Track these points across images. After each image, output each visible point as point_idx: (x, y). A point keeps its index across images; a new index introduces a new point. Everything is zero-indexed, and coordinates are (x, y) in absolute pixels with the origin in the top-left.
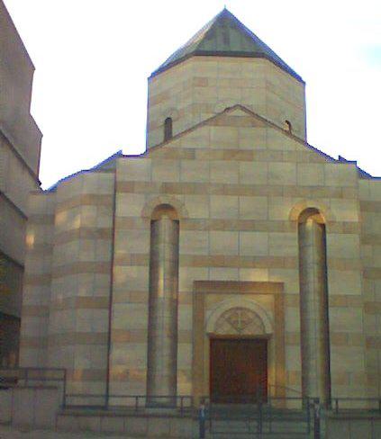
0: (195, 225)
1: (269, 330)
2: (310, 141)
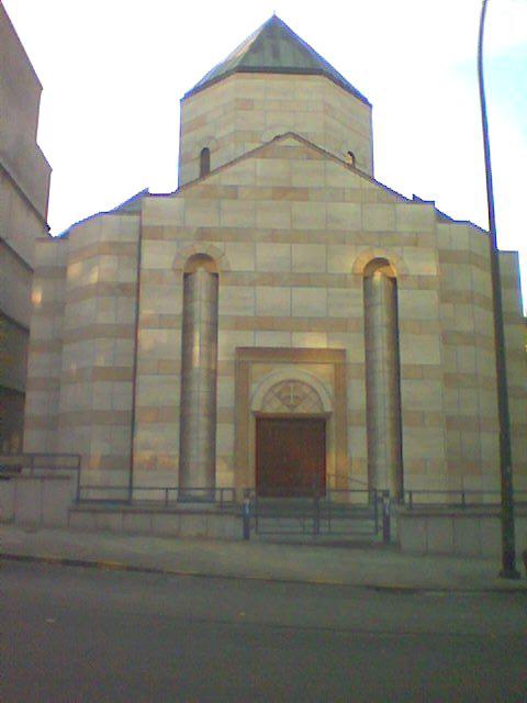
0: (238, 280)
1: (328, 408)
2: (377, 177)
